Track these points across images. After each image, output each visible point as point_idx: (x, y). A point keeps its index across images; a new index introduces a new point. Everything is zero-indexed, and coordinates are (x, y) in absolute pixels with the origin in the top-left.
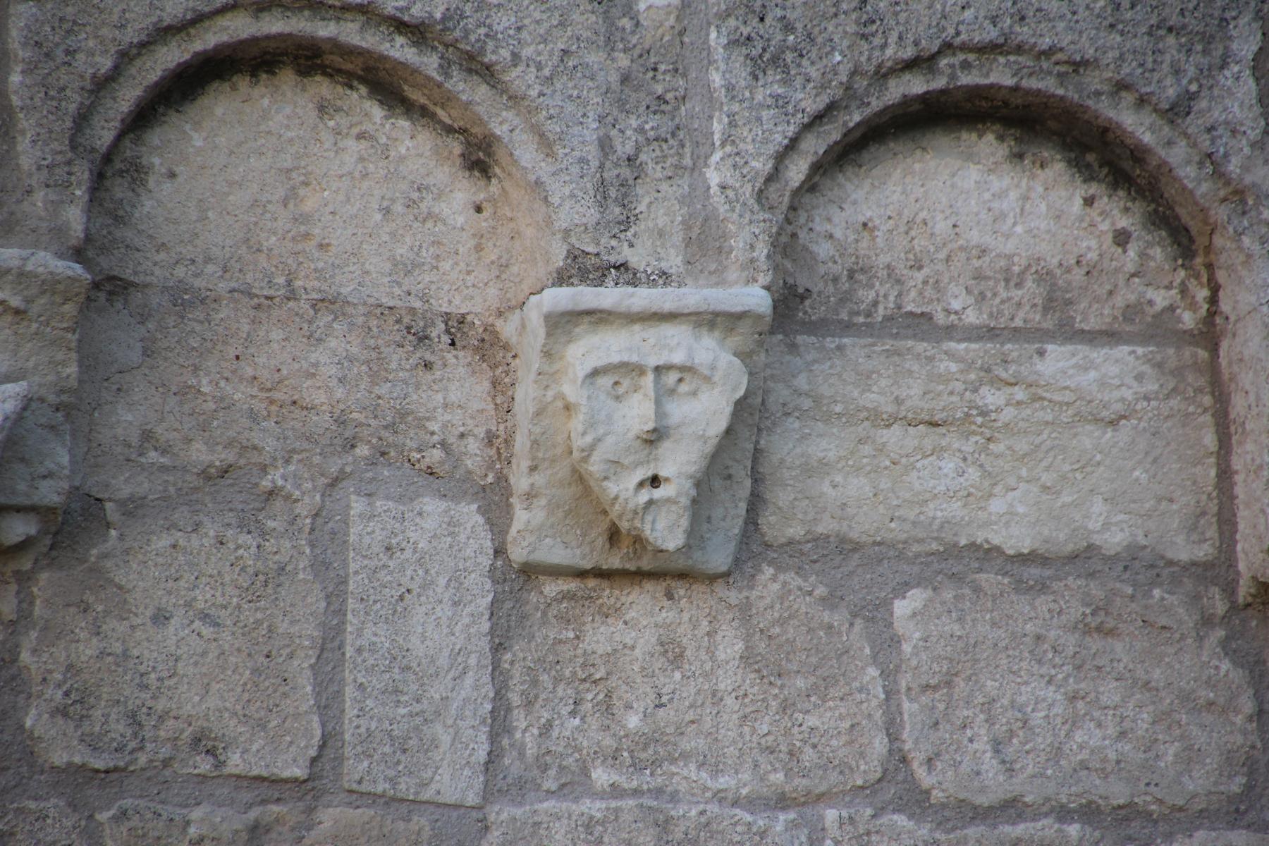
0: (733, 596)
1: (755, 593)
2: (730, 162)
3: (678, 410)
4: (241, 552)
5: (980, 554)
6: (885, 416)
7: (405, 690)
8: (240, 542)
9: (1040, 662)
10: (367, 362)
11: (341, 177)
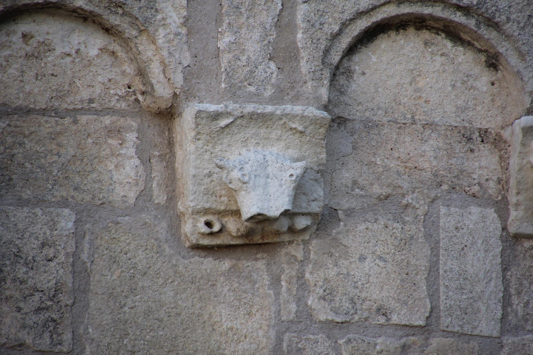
4: (395, 230)
8: (394, 226)
10: (446, 150)
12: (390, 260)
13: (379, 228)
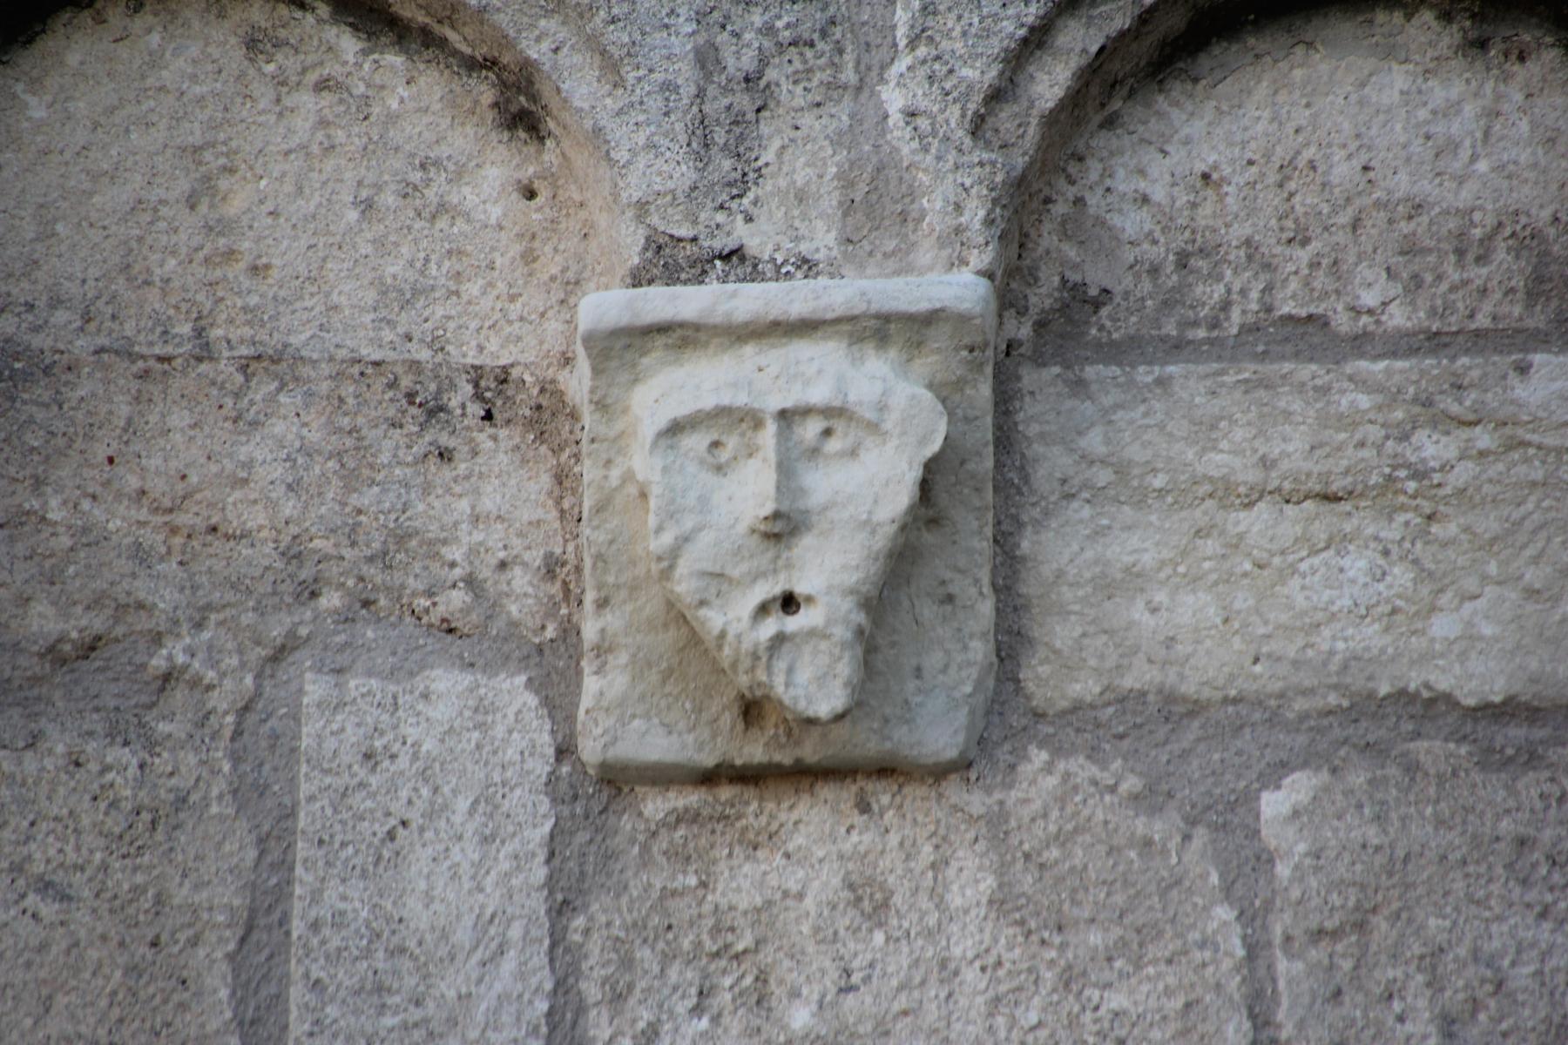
0: (977, 802)
1: (1014, 794)
2: (922, 72)
3: (823, 483)
4: (110, 776)
5: (1418, 709)
6: (1242, 490)
7: (395, 986)
8: (109, 759)
9: (1525, 882)
10: (339, 455)
11: (287, 153)
12: (86, 893)
13: (43, 769)
